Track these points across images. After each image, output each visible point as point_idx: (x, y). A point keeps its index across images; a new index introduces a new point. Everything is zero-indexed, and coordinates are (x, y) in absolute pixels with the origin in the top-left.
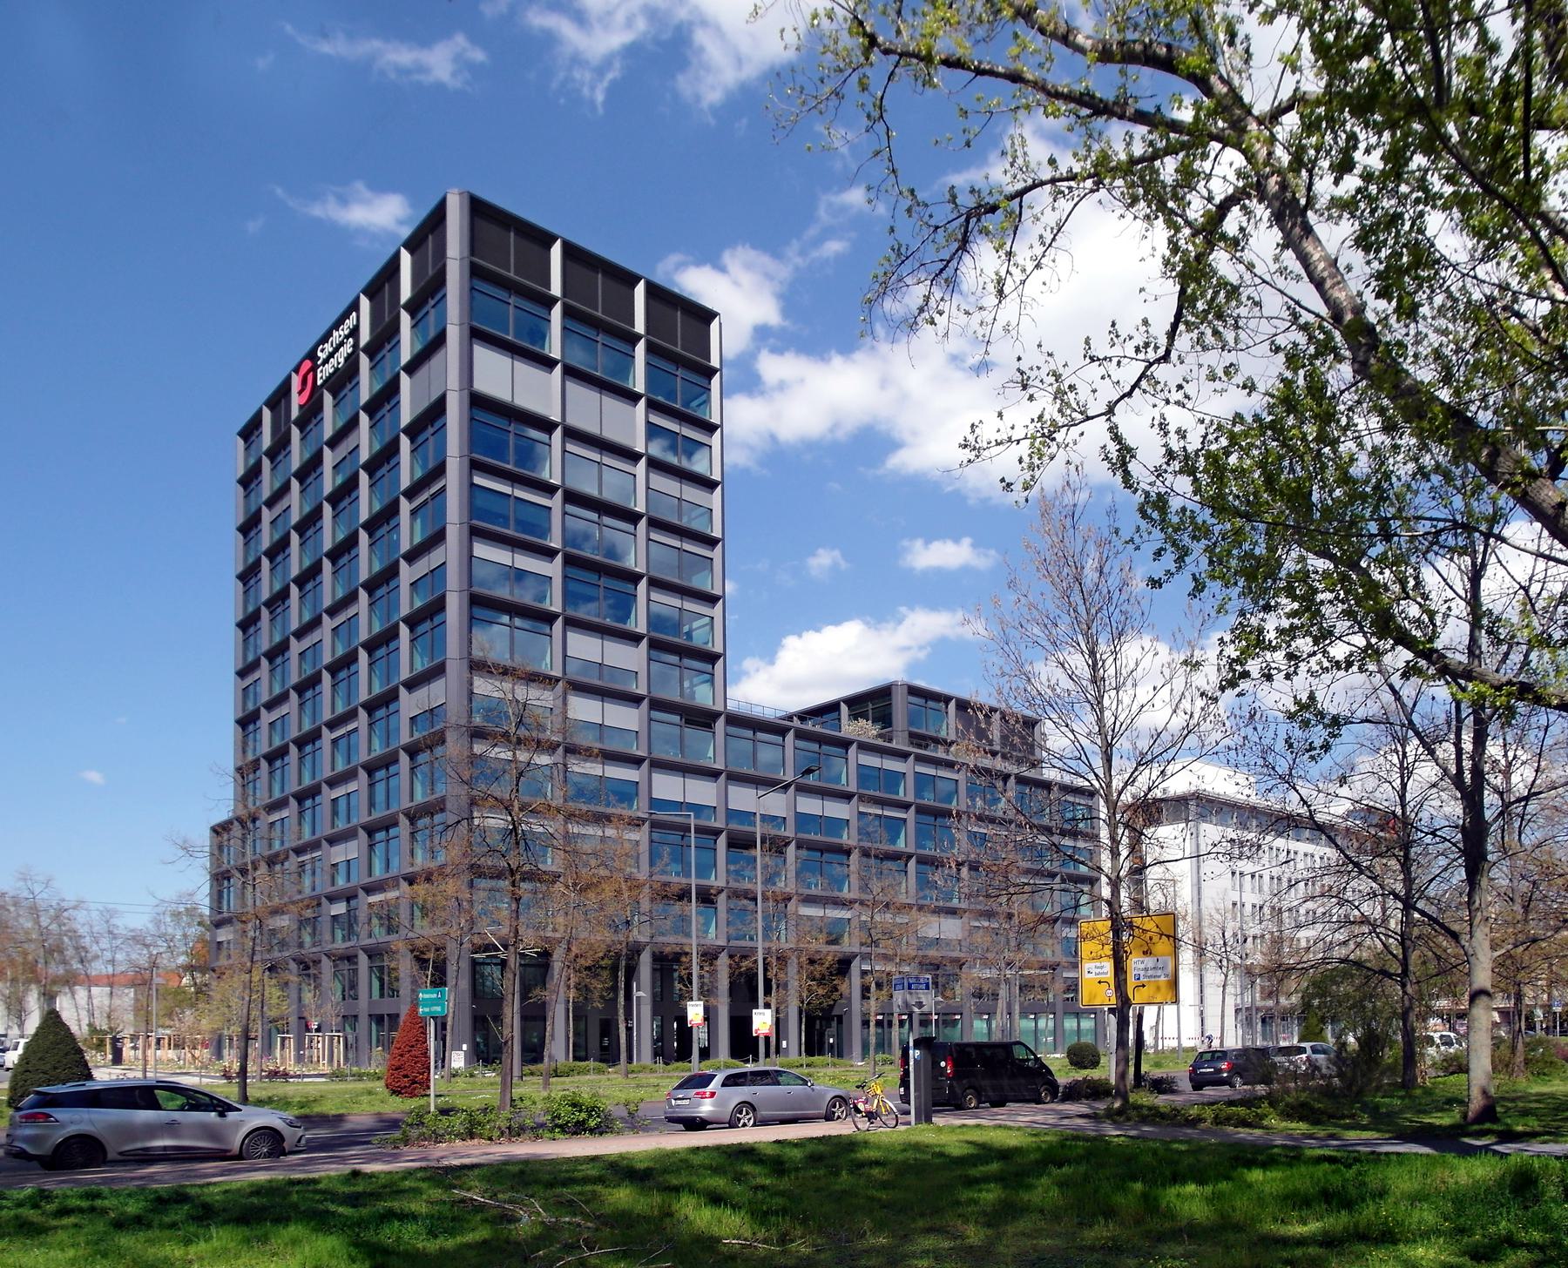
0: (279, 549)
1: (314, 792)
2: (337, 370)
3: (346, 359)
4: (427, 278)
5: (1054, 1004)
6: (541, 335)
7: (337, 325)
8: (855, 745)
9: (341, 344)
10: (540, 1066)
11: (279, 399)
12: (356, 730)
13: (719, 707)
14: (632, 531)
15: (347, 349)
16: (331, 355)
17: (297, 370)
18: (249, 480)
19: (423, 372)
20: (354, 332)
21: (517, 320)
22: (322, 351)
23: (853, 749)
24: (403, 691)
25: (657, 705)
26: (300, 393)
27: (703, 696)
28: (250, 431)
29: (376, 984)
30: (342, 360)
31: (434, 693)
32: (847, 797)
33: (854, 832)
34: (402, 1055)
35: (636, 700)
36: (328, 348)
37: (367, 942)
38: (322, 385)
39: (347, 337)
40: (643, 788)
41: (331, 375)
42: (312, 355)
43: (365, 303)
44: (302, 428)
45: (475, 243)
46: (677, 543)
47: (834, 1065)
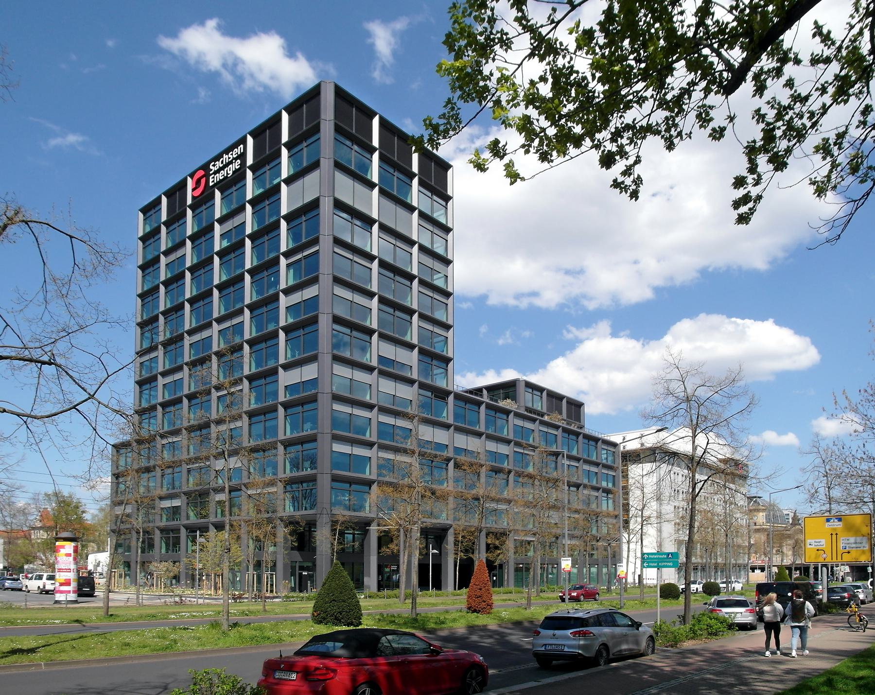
3: (234, 172)
6: (367, 167)
7: (227, 151)
8: (512, 413)
9: (231, 163)
10: (396, 591)
11: (176, 192)
12: (241, 390)
13: (450, 388)
14: (409, 285)
15: (236, 165)
17: (192, 175)
20: (242, 156)
21: (355, 157)
22: (214, 165)
23: (511, 416)
24: (280, 370)
25: (422, 386)
26: (193, 190)
27: (441, 383)
29: (164, 545)
30: (231, 173)
31: (309, 372)
32: (508, 442)
33: (511, 462)
34: (480, 589)
35: (411, 382)
36: (219, 164)
38: (213, 186)
39: (236, 159)
40: (414, 433)
41: (221, 181)
42: (205, 167)
43: (250, 141)
44: (193, 210)
45: (338, 112)
46: (431, 294)
47: (436, 596)
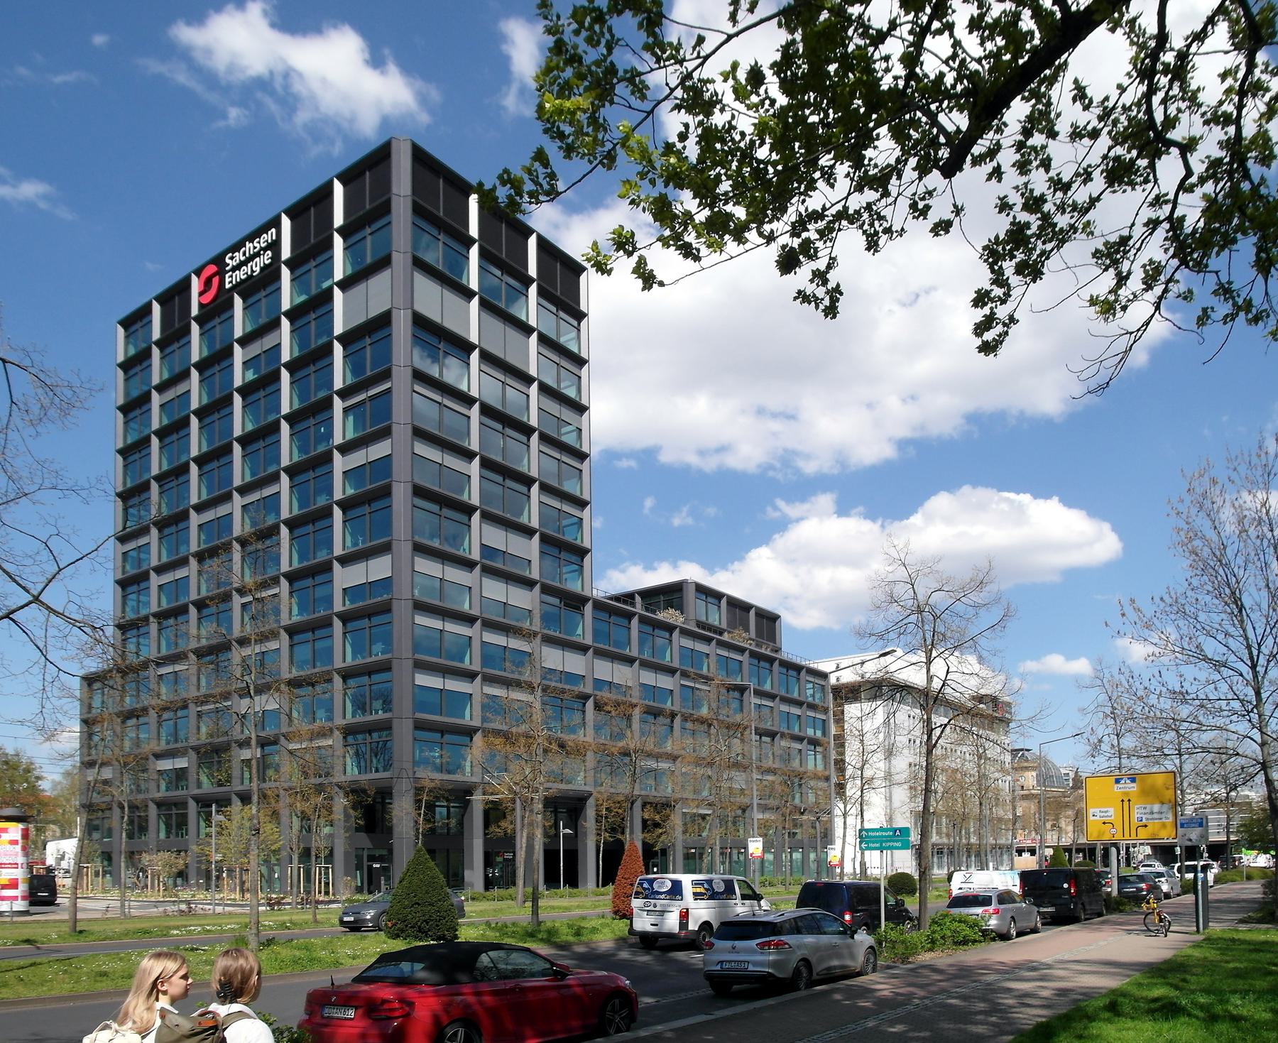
0: (174, 429)
1: (224, 647)
2: (250, 277)
3: (262, 269)
4: (364, 211)
5: (802, 841)
7: (252, 237)
11: (175, 296)
15: (266, 258)
16: (242, 264)
18: (134, 364)
19: (359, 289)
20: (275, 246)
22: (232, 258)
23: (676, 633)
25: (546, 589)
26: (201, 294)
27: (574, 586)
28: (135, 321)
30: (257, 270)
32: (671, 671)
36: (239, 257)
37: (196, 791)
38: (234, 288)
39: (265, 249)
42: (219, 261)
43: (286, 223)
